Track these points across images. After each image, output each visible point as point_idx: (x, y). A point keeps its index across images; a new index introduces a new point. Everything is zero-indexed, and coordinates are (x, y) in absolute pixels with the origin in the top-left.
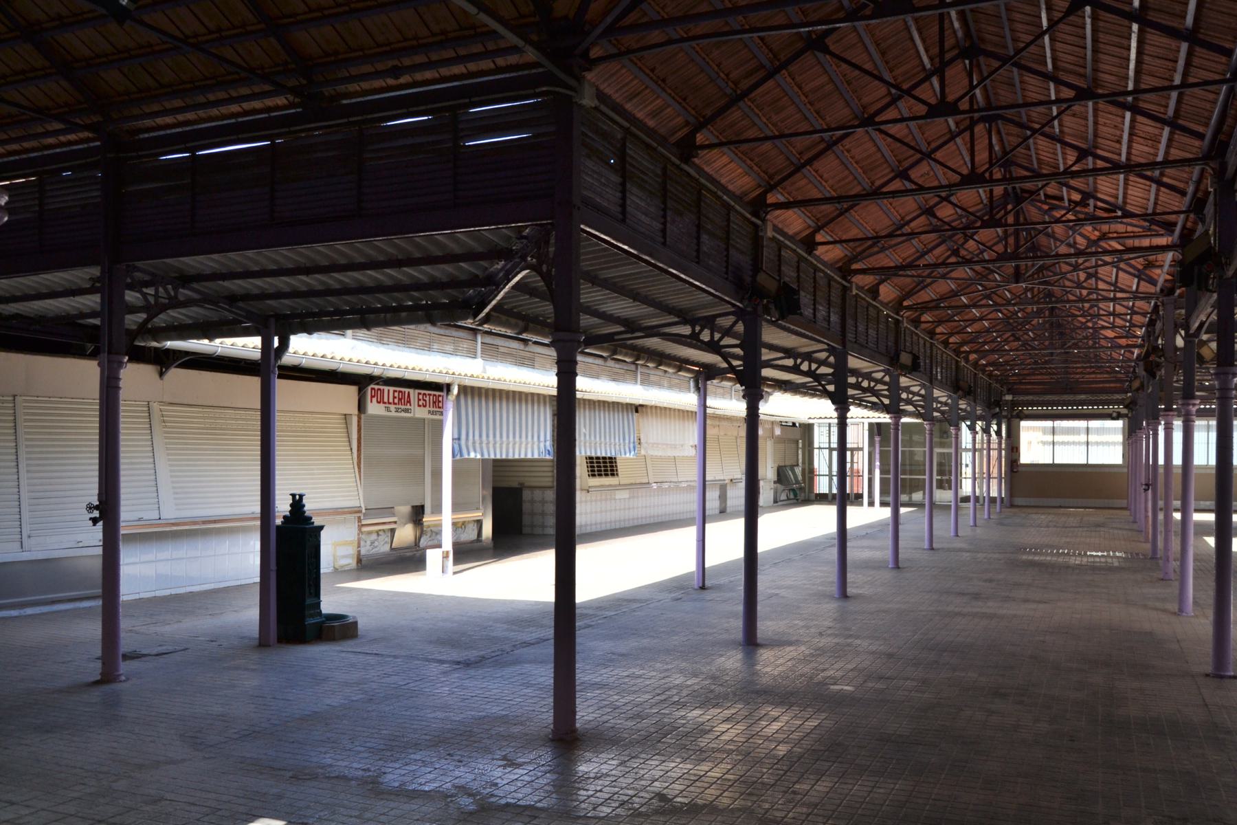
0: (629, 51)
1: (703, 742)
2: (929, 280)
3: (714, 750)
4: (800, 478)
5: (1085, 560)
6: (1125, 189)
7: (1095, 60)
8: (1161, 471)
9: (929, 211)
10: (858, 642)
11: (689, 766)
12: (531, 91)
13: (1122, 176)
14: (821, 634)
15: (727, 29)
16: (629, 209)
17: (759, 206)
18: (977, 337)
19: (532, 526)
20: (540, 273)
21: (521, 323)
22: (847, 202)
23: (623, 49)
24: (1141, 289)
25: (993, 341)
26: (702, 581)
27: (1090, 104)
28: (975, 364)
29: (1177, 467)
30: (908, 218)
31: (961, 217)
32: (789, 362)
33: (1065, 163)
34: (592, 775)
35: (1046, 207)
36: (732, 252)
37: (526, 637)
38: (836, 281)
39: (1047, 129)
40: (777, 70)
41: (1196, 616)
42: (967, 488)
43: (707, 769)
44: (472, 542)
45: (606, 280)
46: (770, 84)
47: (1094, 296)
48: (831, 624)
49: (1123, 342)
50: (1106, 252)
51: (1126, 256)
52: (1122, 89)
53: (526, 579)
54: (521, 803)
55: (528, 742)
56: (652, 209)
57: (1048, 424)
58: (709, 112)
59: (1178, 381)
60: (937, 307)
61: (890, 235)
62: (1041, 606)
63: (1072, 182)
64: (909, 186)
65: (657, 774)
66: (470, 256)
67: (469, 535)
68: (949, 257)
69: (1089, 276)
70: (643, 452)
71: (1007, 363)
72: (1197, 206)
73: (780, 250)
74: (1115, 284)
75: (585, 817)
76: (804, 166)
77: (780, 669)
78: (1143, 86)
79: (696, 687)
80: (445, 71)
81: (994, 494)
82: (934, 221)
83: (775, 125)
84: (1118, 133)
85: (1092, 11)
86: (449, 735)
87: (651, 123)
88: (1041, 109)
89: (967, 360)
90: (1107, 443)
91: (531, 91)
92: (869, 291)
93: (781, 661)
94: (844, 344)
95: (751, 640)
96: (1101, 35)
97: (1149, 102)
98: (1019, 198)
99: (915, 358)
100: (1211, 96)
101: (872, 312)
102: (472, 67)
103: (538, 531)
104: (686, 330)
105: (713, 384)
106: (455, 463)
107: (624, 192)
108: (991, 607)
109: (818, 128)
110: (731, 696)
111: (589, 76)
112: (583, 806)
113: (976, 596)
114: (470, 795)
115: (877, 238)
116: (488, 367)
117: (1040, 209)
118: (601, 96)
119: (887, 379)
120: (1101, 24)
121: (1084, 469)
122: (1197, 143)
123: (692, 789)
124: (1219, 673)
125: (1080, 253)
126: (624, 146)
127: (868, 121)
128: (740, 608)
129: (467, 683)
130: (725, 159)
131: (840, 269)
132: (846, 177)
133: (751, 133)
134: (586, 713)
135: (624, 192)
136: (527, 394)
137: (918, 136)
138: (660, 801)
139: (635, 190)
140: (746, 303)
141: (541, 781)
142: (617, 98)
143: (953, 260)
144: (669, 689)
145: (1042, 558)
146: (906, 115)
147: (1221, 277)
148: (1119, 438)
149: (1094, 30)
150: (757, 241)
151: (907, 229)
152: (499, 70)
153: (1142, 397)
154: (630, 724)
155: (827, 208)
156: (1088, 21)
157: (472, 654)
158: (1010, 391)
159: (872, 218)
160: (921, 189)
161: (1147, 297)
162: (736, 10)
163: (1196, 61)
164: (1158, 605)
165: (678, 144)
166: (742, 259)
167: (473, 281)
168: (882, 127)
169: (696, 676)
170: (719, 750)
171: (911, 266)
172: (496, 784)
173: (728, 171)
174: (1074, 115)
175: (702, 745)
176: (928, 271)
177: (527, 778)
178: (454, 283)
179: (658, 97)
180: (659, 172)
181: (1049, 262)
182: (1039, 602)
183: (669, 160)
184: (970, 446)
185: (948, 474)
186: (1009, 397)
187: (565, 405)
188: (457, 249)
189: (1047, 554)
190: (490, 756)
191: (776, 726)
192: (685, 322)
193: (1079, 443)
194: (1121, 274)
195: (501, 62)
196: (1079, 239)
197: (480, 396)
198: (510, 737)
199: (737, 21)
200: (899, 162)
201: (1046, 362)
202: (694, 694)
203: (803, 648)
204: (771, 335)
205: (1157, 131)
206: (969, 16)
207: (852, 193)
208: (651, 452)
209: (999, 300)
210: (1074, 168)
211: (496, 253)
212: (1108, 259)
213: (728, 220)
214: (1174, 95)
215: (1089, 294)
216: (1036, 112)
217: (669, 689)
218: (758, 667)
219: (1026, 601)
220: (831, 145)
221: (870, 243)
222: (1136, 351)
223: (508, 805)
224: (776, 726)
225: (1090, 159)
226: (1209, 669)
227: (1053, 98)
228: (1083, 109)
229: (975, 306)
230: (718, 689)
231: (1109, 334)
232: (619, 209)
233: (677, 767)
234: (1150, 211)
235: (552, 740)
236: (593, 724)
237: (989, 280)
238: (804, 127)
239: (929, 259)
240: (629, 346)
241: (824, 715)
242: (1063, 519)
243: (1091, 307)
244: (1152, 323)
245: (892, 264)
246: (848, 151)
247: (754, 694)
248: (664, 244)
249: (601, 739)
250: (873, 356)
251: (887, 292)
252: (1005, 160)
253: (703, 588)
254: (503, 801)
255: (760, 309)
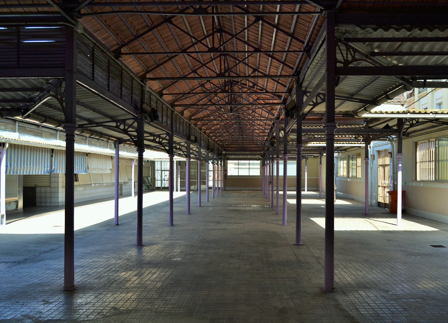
0: (96, 13)
1: (128, 285)
2: (201, 110)
3: (133, 288)
4: (150, 181)
5: (251, 208)
6: (267, 83)
7: (261, 39)
8: (275, 178)
9: (203, 85)
10: (180, 242)
11: (124, 295)
12: (55, 23)
13: (266, 79)
14: (166, 240)
15: (135, 10)
16: (95, 75)
17: (143, 78)
18: (215, 131)
19: (41, 203)
20: (57, 99)
21: (43, 119)
22: (175, 79)
23: (94, 12)
24: (269, 117)
25: (220, 133)
26: (117, 222)
27: (258, 54)
28: (214, 140)
29: (281, 176)
30: (195, 87)
31: (213, 88)
32: (152, 138)
33: (248, 73)
34: (84, 303)
35: (240, 87)
36: (134, 95)
37: (45, 249)
38: (170, 108)
39: (244, 61)
40: (153, 28)
41: (288, 225)
42: (211, 184)
43: (131, 295)
44: (13, 210)
45: (82, 103)
46: (150, 33)
47: (254, 119)
48: (169, 236)
49: (261, 134)
50: (259, 104)
51: (265, 106)
52: (269, 50)
53: (50, 223)
54: (54, 319)
55: (53, 293)
56: (104, 76)
57: (237, 162)
58: (126, 41)
59: (282, 147)
60: (203, 120)
61: (189, 93)
62: (240, 225)
63: (250, 79)
64: (197, 76)
65: (111, 299)
66: (23, 89)
67: (13, 207)
68: (208, 102)
69: (253, 112)
70: (89, 172)
71: (224, 140)
72: (290, 91)
73: (150, 96)
74: (261, 115)
75: (84, 321)
76: (160, 65)
77: (153, 254)
78: (276, 50)
79: (121, 264)
80: (13, 10)
81: (219, 186)
82: (204, 89)
83: (151, 48)
84: (266, 64)
85: (262, 23)
86: (15, 294)
87: (103, 42)
88: (242, 54)
89: (211, 139)
90: (245, 168)
91: (55, 23)
92: (180, 112)
93: (153, 251)
94: (172, 132)
95: (140, 244)
96: (264, 31)
97: (277, 55)
98: (232, 83)
99: (196, 137)
100: (296, 56)
101: (181, 120)
102: (27, 9)
103: (43, 204)
104: (114, 124)
105: (121, 145)
106: (7, 176)
107: (93, 68)
108: (223, 226)
109: (167, 51)
110: (136, 266)
111: (80, 20)
112: (82, 316)
113: (218, 223)
114: (30, 318)
115: (184, 94)
116: (21, 136)
117: (238, 88)
118: (85, 30)
119: (186, 145)
120: (264, 27)
121: (248, 177)
122: (290, 70)
123: (126, 304)
124: (298, 243)
125: (251, 104)
126: (93, 50)
127: (184, 51)
128: (136, 231)
129: (20, 271)
130: (131, 59)
131: (171, 104)
132: (175, 71)
133: (142, 51)
134: (78, 279)
135: (93, 68)
136: (40, 148)
137: (200, 58)
138: (114, 310)
139: (97, 68)
140: (139, 115)
141: (61, 308)
142: (91, 30)
143: (209, 103)
144: (110, 265)
145: (238, 208)
146: (197, 51)
147: (298, 114)
148: (259, 167)
149: (262, 29)
150: (142, 92)
151: (194, 91)
152: (39, 12)
153: (267, 151)
154: (96, 281)
155: (168, 81)
156: (260, 26)
157: (21, 258)
158: (225, 150)
159: (183, 86)
160: (201, 77)
161: (271, 120)
162: (139, 3)
163: (292, 43)
164: (276, 222)
165: (114, 51)
166: (137, 98)
167: (23, 100)
168: (190, 54)
169: (120, 259)
170: (134, 287)
171: (194, 105)
172: (41, 312)
173: (132, 64)
174: (252, 57)
175: (128, 286)
176: (200, 107)
177: (55, 308)
178: (14, 100)
179: (107, 32)
180: (107, 62)
181: (239, 106)
182: (239, 223)
183: (111, 57)
184: (212, 169)
185: (204, 179)
186: (224, 152)
187: (70, 153)
188: (17, 86)
189: (239, 207)
190: (37, 301)
191: (155, 276)
192: (113, 121)
193: (246, 168)
194: (263, 111)
195: (40, 9)
196: (250, 99)
197: (18, 148)
198: (44, 292)
199: (139, 8)
200: (194, 67)
201: (236, 140)
202: (121, 267)
203: (160, 245)
204: (147, 128)
205: (278, 65)
206: (220, 18)
207: (177, 77)
208: (93, 172)
209: (223, 118)
210: (251, 75)
211: (35, 89)
212: (259, 106)
213: (132, 83)
214: (285, 54)
215: (252, 118)
216: (240, 54)
217: (110, 265)
218: (144, 254)
219: (235, 223)
220: (170, 59)
221: (181, 95)
222: (266, 138)
223: (48, 320)
224: (155, 276)
225: (257, 72)
226: (295, 243)
227: (246, 50)
228: (256, 55)
229: (215, 120)
230: (130, 264)
231: (257, 131)
232: (92, 75)
233: (120, 296)
234: (274, 91)
235: (64, 291)
236: (81, 283)
237: (221, 111)
238: (162, 51)
239: (201, 102)
240: (92, 130)
241: (172, 270)
242: (242, 194)
243: (253, 122)
244: (272, 128)
245: (189, 104)
246: (176, 61)
247: (141, 264)
248: (109, 90)
249: (85, 288)
250: (182, 136)
251: (187, 113)
252: (228, 70)
253: (117, 225)
254: (46, 319)
255: (143, 117)
